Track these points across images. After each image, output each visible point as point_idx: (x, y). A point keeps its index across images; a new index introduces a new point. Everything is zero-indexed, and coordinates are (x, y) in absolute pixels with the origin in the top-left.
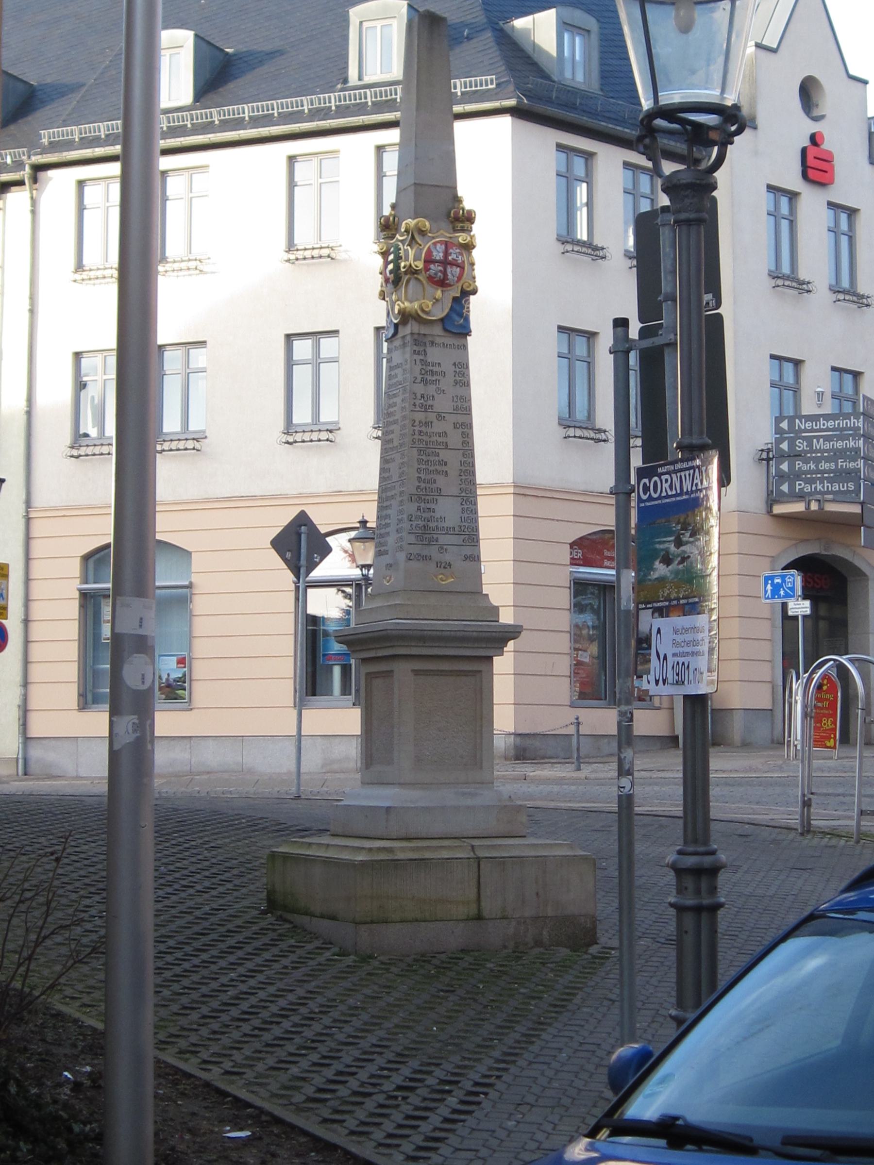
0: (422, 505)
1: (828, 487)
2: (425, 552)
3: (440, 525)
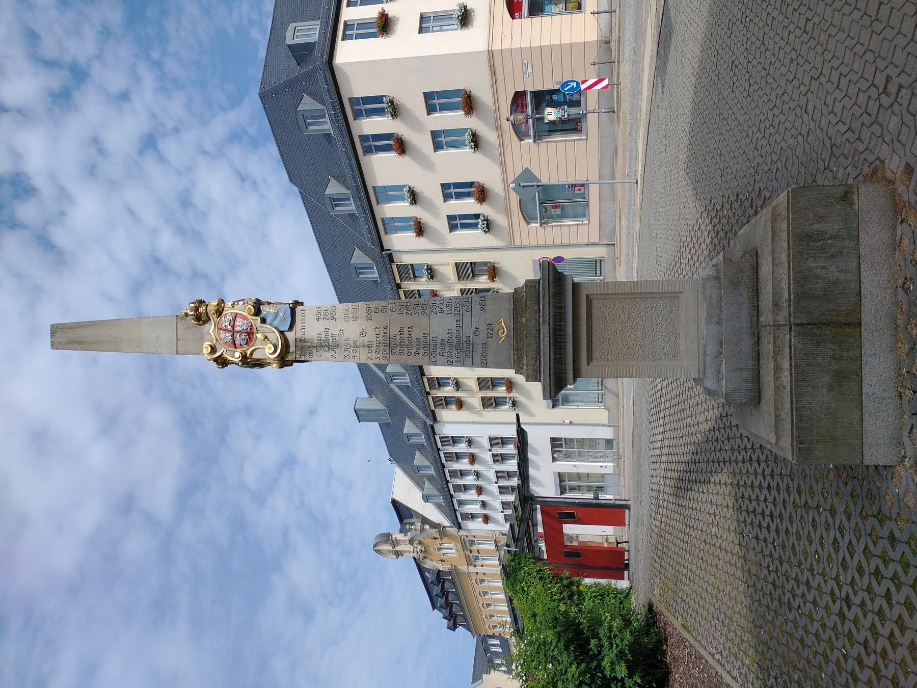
0: (439, 351)
2: (479, 349)
3: (454, 334)
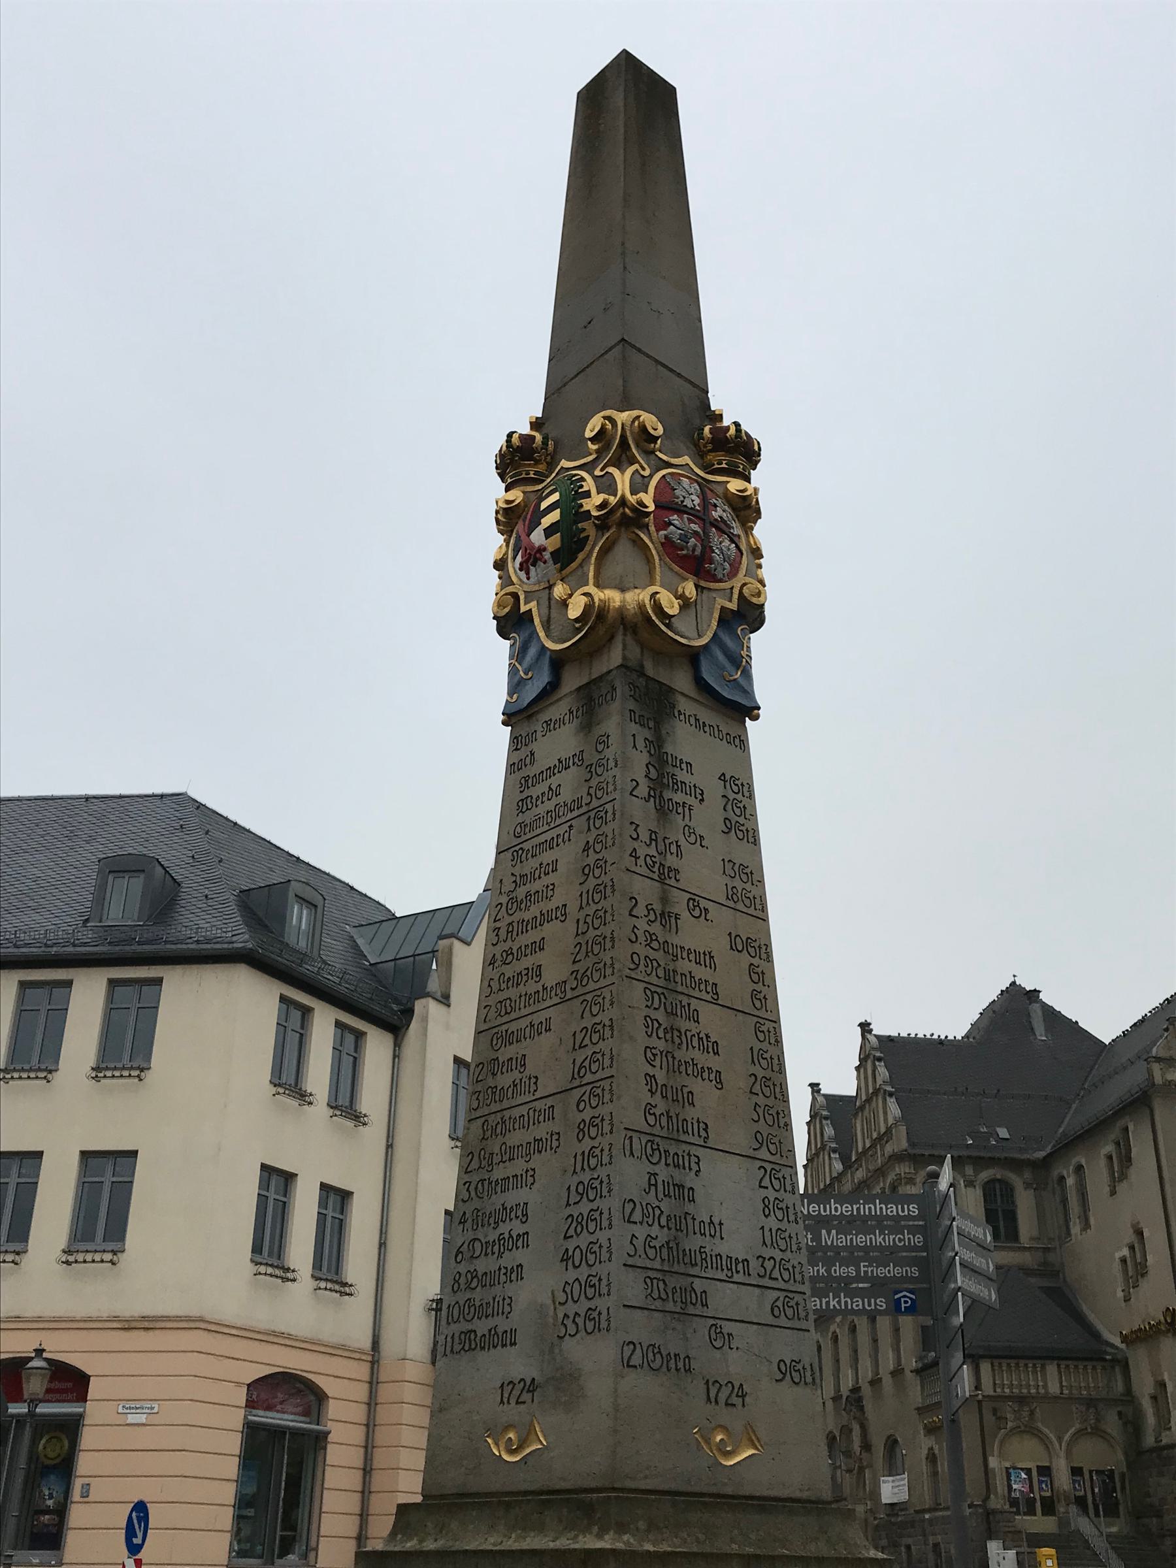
0: (663, 1172)
1: (846, 1302)
